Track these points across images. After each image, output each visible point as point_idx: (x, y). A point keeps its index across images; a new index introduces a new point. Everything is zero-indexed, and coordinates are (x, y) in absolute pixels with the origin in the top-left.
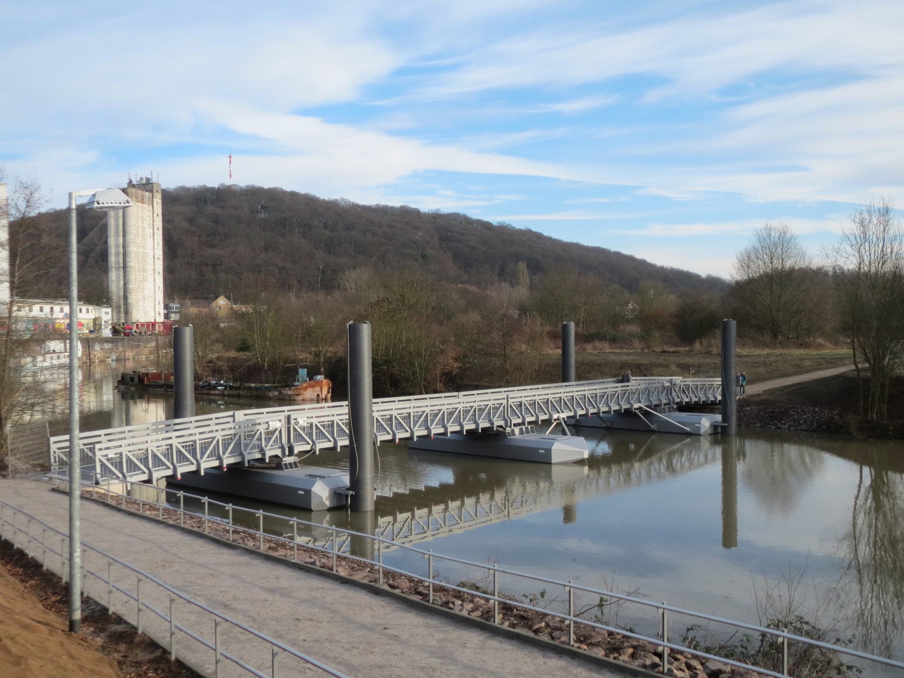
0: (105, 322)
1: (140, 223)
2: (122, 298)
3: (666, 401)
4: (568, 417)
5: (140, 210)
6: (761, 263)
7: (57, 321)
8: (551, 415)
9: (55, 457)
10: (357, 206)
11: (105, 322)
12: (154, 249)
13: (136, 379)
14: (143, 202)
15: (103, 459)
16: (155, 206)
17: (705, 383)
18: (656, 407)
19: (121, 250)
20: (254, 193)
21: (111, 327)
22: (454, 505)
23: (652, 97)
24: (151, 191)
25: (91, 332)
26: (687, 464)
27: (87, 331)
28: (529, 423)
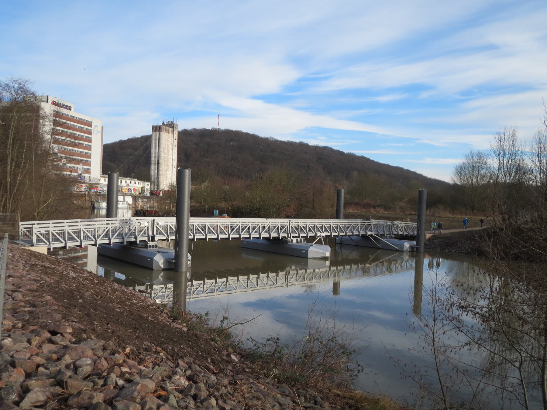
0: (147, 189)
1: (167, 143)
2: (156, 178)
3: (388, 233)
4: (326, 236)
5: (167, 136)
6: (467, 171)
7: (123, 187)
8: (316, 234)
9: (22, 232)
10: (278, 141)
11: (147, 189)
12: (173, 155)
13: (142, 213)
14: (168, 133)
15: (38, 233)
16: (174, 135)
17: (413, 225)
18: (381, 235)
19: (157, 155)
20: (228, 133)
21: (149, 192)
22: (253, 277)
23: (424, 95)
24: (173, 127)
25: (140, 193)
26: (399, 268)
27: (138, 193)
28: (302, 237)
